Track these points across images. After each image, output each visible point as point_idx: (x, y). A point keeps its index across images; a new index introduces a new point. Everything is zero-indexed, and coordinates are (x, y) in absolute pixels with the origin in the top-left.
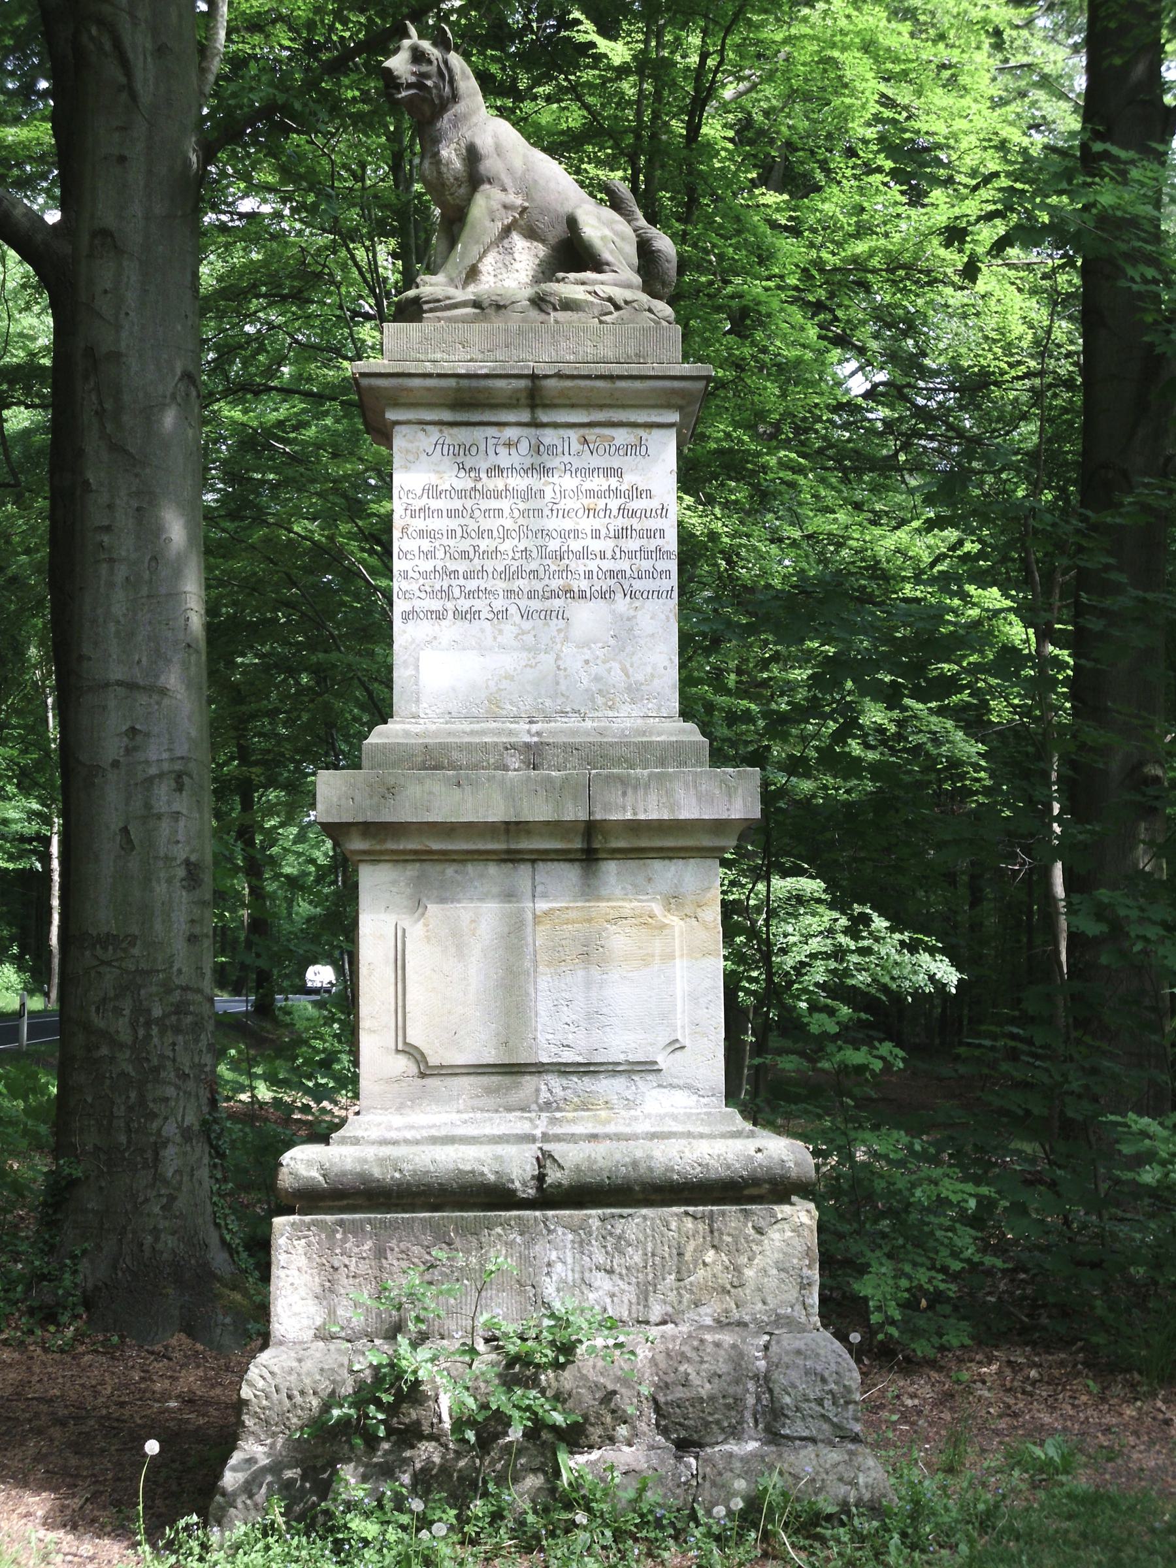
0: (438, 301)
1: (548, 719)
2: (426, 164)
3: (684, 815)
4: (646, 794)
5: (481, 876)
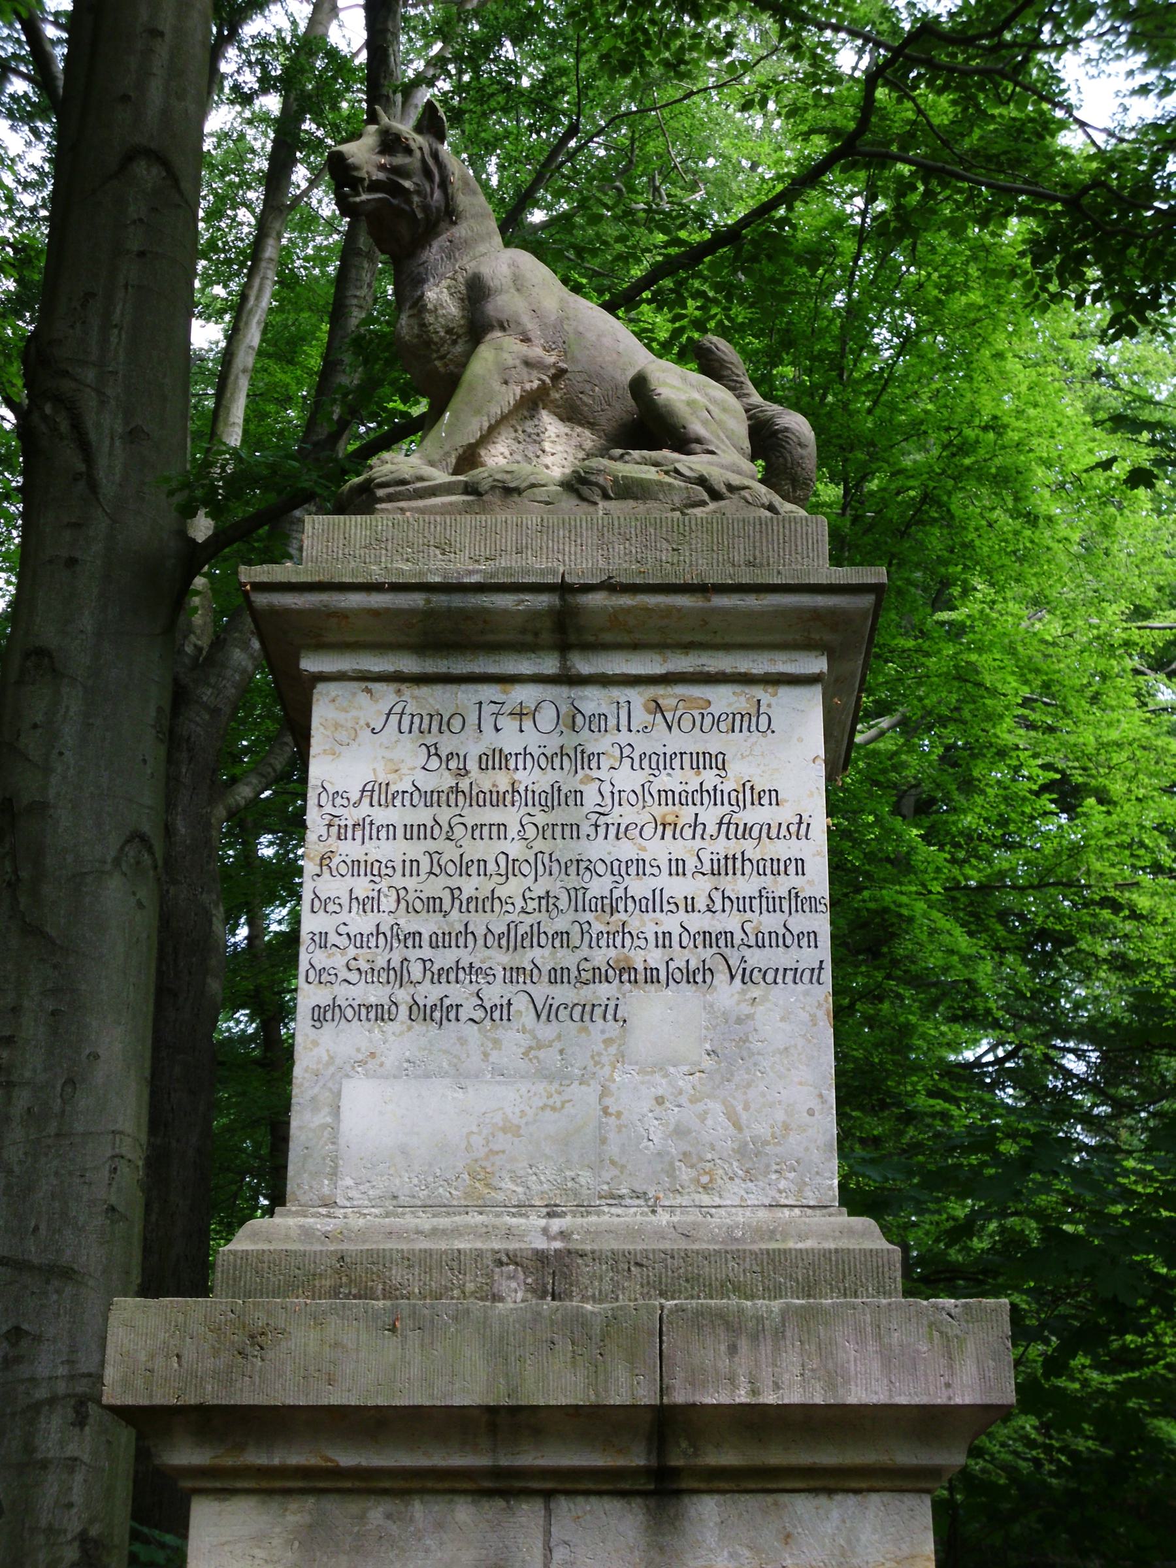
0: (403, 482)
1: (584, 1208)
2: (404, 320)
3: (856, 1395)
4: (777, 1350)
5: (440, 1526)
